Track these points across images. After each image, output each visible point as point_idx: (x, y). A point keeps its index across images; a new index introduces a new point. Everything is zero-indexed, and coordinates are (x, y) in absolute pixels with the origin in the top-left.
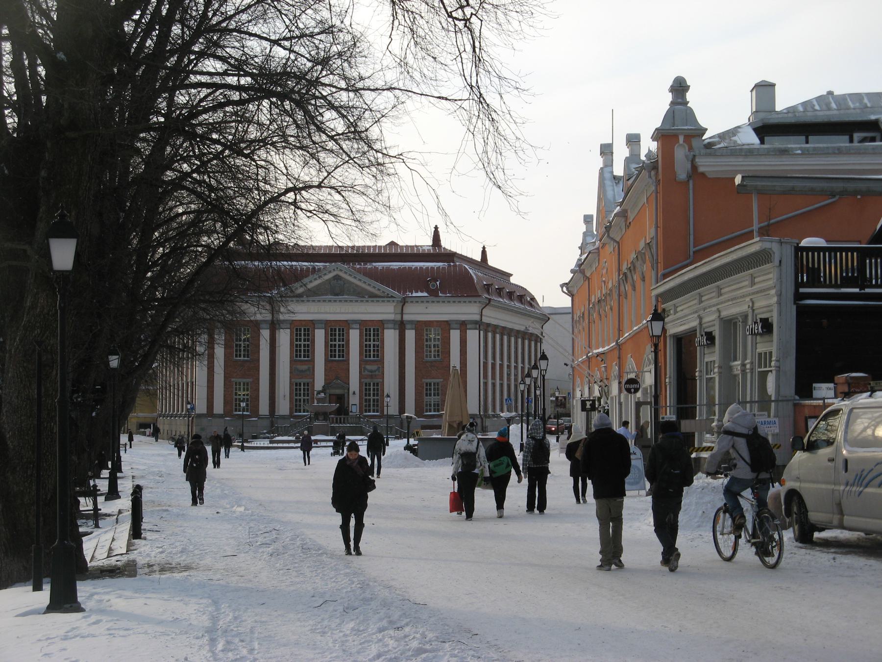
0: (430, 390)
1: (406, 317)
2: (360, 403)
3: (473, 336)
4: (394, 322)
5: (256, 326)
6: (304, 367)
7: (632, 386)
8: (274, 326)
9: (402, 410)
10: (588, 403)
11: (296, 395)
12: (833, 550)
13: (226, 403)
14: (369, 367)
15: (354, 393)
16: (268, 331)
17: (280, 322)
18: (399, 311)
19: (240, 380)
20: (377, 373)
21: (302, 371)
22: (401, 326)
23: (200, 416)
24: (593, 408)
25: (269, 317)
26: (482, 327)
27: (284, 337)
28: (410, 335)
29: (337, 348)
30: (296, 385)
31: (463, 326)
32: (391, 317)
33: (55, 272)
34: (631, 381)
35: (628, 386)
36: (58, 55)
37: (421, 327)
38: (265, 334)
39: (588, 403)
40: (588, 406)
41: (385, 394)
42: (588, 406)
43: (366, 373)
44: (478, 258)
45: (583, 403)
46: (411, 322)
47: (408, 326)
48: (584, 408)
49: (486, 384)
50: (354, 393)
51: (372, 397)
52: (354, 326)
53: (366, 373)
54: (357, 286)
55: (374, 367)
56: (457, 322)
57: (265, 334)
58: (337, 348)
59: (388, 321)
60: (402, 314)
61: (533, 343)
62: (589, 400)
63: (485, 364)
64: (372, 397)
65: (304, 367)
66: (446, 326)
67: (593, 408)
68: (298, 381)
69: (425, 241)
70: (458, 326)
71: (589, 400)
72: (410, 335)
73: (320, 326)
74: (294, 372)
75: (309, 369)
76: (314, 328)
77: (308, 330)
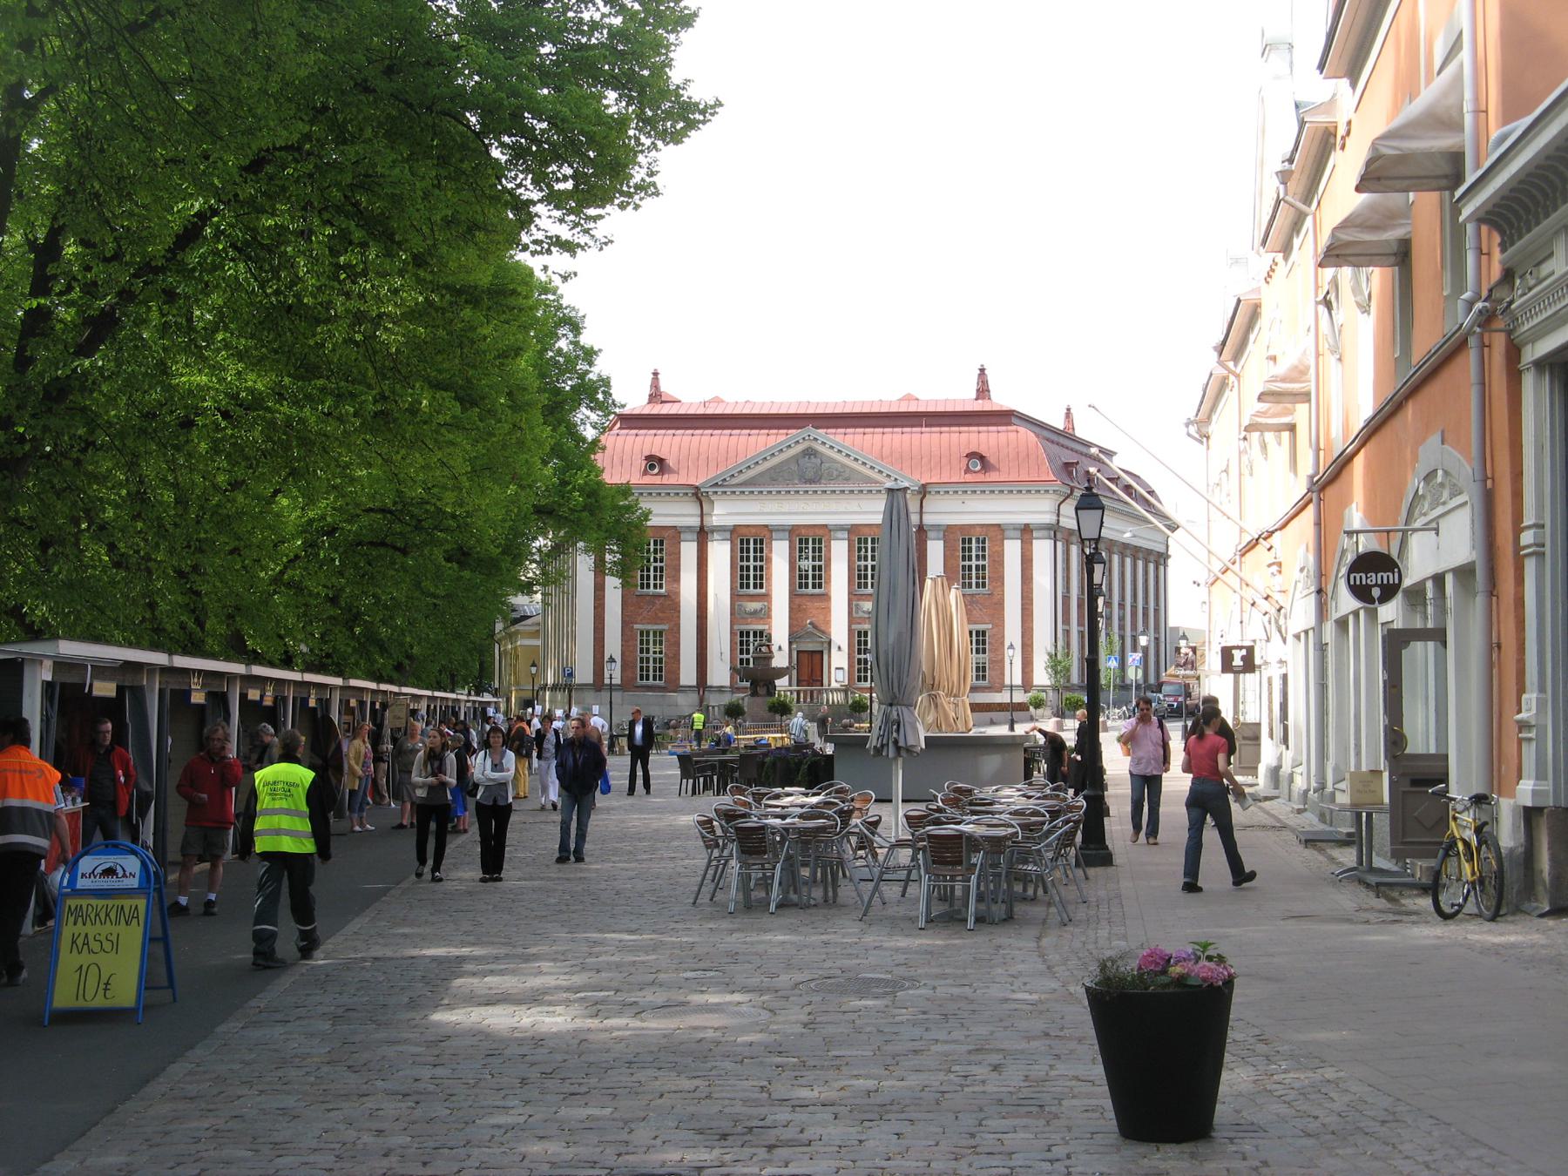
1: (929, 519)
2: (850, 666)
3: (1043, 549)
5: (676, 533)
7: (1373, 578)
8: (703, 535)
10: (1238, 656)
19: (649, 627)
23: (583, 687)
24: (1249, 665)
25: (695, 521)
26: (1059, 535)
27: (720, 554)
31: (1026, 532)
34: (1370, 562)
35: (1361, 578)
38: (689, 550)
39: (1238, 656)
40: (1237, 662)
42: (1237, 662)
44: (1059, 424)
45: (1227, 653)
46: (936, 527)
47: (930, 534)
48: (1227, 666)
49: (1067, 633)
54: (844, 466)
56: (1015, 527)
57: (689, 550)
61: (1151, 566)
62: (1240, 648)
66: (999, 531)
67: (1249, 665)
68: (744, 627)
69: (961, 395)
70: (1018, 534)
71: (1240, 648)
73: (781, 535)
74: (736, 614)
76: (771, 539)
77: (762, 542)
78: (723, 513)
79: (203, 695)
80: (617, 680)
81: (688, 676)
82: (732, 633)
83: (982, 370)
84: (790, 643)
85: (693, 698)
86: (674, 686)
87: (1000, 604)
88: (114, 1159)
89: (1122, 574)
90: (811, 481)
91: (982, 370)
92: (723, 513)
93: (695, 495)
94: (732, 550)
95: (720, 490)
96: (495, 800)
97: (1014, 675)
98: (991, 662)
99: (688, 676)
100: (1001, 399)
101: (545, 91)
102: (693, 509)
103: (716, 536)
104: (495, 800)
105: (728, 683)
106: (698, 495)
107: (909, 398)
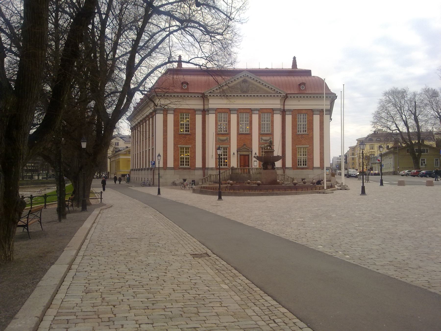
1: (286, 107)
4: (279, 110)
6: (224, 138)
8: (205, 112)
12: (311, 247)
13: (175, 160)
14: (264, 138)
17: (208, 110)
18: (283, 103)
20: (226, 141)
21: (223, 141)
22: (283, 112)
25: (201, 107)
28: (289, 118)
29: (266, 126)
32: (279, 106)
36: (59, 13)
37: (296, 113)
38: (199, 118)
41: (157, 155)
43: (263, 141)
52: (255, 112)
53: (263, 141)
57: (199, 118)
58: (266, 126)
59: (277, 109)
60: (284, 105)
63: (153, 139)
65: (224, 138)
66: (311, 112)
69: (288, 66)
73: (234, 112)
74: (218, 141)
75: (227, 139)
79: (61, 23)
80: (172, 166)
81: (199, 164)
84: (237, 152)
85: (200, 172)
86: (193, 168)
87: (312, 138)
88: (1, 181)
89: (143, 144)
90: (244, 92)
91: (294, 58)
99: (199, 164)
100: (300, 66)
101: (49, 88)
105: (214, 167)
106: (204, 97)
107: (266, 68)
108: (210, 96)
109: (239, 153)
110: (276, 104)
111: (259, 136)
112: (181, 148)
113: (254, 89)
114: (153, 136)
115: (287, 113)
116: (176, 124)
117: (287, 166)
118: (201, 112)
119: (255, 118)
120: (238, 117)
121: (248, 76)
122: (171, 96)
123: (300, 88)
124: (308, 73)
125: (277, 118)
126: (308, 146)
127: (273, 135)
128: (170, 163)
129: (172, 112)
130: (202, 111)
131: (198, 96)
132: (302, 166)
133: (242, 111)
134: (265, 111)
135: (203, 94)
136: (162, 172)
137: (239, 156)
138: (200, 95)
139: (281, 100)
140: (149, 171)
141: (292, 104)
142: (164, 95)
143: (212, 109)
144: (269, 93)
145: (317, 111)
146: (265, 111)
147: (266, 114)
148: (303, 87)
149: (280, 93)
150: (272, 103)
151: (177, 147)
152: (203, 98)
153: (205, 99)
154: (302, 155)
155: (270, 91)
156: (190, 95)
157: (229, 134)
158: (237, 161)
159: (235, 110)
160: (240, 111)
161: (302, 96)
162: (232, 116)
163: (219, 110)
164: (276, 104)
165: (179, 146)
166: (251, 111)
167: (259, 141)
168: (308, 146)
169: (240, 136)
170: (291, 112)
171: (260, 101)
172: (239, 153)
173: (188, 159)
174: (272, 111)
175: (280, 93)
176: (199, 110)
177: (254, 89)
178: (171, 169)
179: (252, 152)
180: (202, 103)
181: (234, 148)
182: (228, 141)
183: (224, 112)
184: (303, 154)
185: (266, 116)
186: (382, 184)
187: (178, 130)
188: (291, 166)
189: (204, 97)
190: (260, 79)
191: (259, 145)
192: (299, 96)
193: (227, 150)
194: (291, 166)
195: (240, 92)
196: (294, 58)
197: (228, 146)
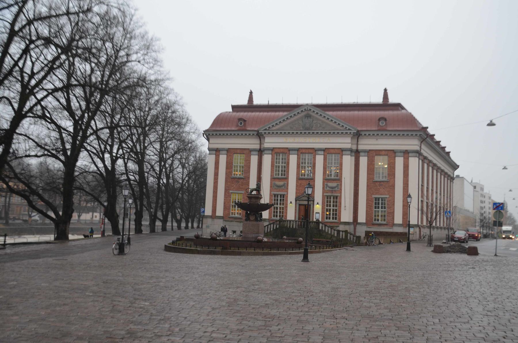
0: (379, 204)
1: (361, 147)
3: (414, 162)
4: (351, 150)
6: (281, 183)
8: (261, 152)
9: (422, 223)
11: (336, 210)
14: (330, 184)
15: (291, 203)
16: (257, 156)
20: (336, 189)
22: (357, 153)
25: (257, 147)
28: (364, 161)
30: (275, 195)
31: (406, 154)
32: (349, 146)
33: (374, 157)
37: (372, 154)
38: (254, 159)
43: (328, 188)
46: (365, 151)
50: (291, 203)
51: (332, 208)
52: (320, 152)
53: (328, 188)
55: (334, 184)
56: (401, 151)
57: (254, 159)
60: (357, 144)
64: (332, 208)
65: (281, 183)
69: (379, 99)
72: (364, 161)
75: (284, 185)
78: (270, 142)
82: (271, 195)
83: (251, 93)
84: (296, 200)
87: (393, 186)
91: (385, 90)
92: (270, 142)
93: (257, 135)
94: (272, 159)
95: (267, 132)
96: (306, 259)
97: (398, 219)
98: (388, 213)
100: (392, 100)
102: (257, 141)
103: (266, 152)
104: (306, 259)
106: (260, 136)
108: (265, 133)
109: (298, 202)
110: (346, 142)
111: (323, 182)
112: (376, 199)
113: (319, 125)
114: (422, 186)
115: (361, 154)
116: (229, 166)
117: (359, 221)
118: (257, 153)
119: (320, 159)
120: (298, 158)
121: (310, 110)
122: (224, 134)
123: (379, 123)
124: (398, 106)
125: (348, 161)
126: (388, 196)
127: (314, 181)
128: (220, 212)
129: (225, 152)
130: (259, 151)
131: (253, 134)
132: (380, 222)
133: (304, 151)
134: (332, 151)
135: (258, 131)
136: (209, 221)
137: (298, 206)
138: (255, 133)
139: (352, 138)
140: (443, 230)
141: (366, 144)
142: (213, 134)
143: (268, 149)
144: (337, 130)
145: (400, 152)
146: (332, 151)
147: (333, 155)
148: (241, 124)
149: (349, 129)
150: (340, 141)
151: (229, 193)
152: (259, 136)
153: (261, 137)
154: (332, 206)
155: (338, 127)
156: (248, 133)
157: (287, 179)
158: (295, 213)
159: (295, 150)
160: (301, 151)
161: (384, 133)
162: (317, 157)
163: (276, 151)
164: (346, 142)
165: (373, 196)
166: (314, 151)
167: (323, 188)
168: (388, 196)
169: (300, 182)
170: (367, 153)
171: (326, 140)
172: (298, 202)
173: (336, 211)
174: (341, 151)
175: (349, 129)
176: (254, 150)
177: (319, 125)
178: (219, 217)
179: (314, 201)
180: (258, 142)
181: (292, 195)
182: (286, 187)
183: (283, 153)
184: (280, 203)
185: (307, 157)
186: (409, 249)
187: (231, 173)
188: (364, 221)
189: (260, 136)
190: (328, 115)
191: (323, 193)
192: (380, 133)
193: (310, 198)
194: (364, 221)
195: (302, 129)
196: (385, 90)
197: (286, 193)
